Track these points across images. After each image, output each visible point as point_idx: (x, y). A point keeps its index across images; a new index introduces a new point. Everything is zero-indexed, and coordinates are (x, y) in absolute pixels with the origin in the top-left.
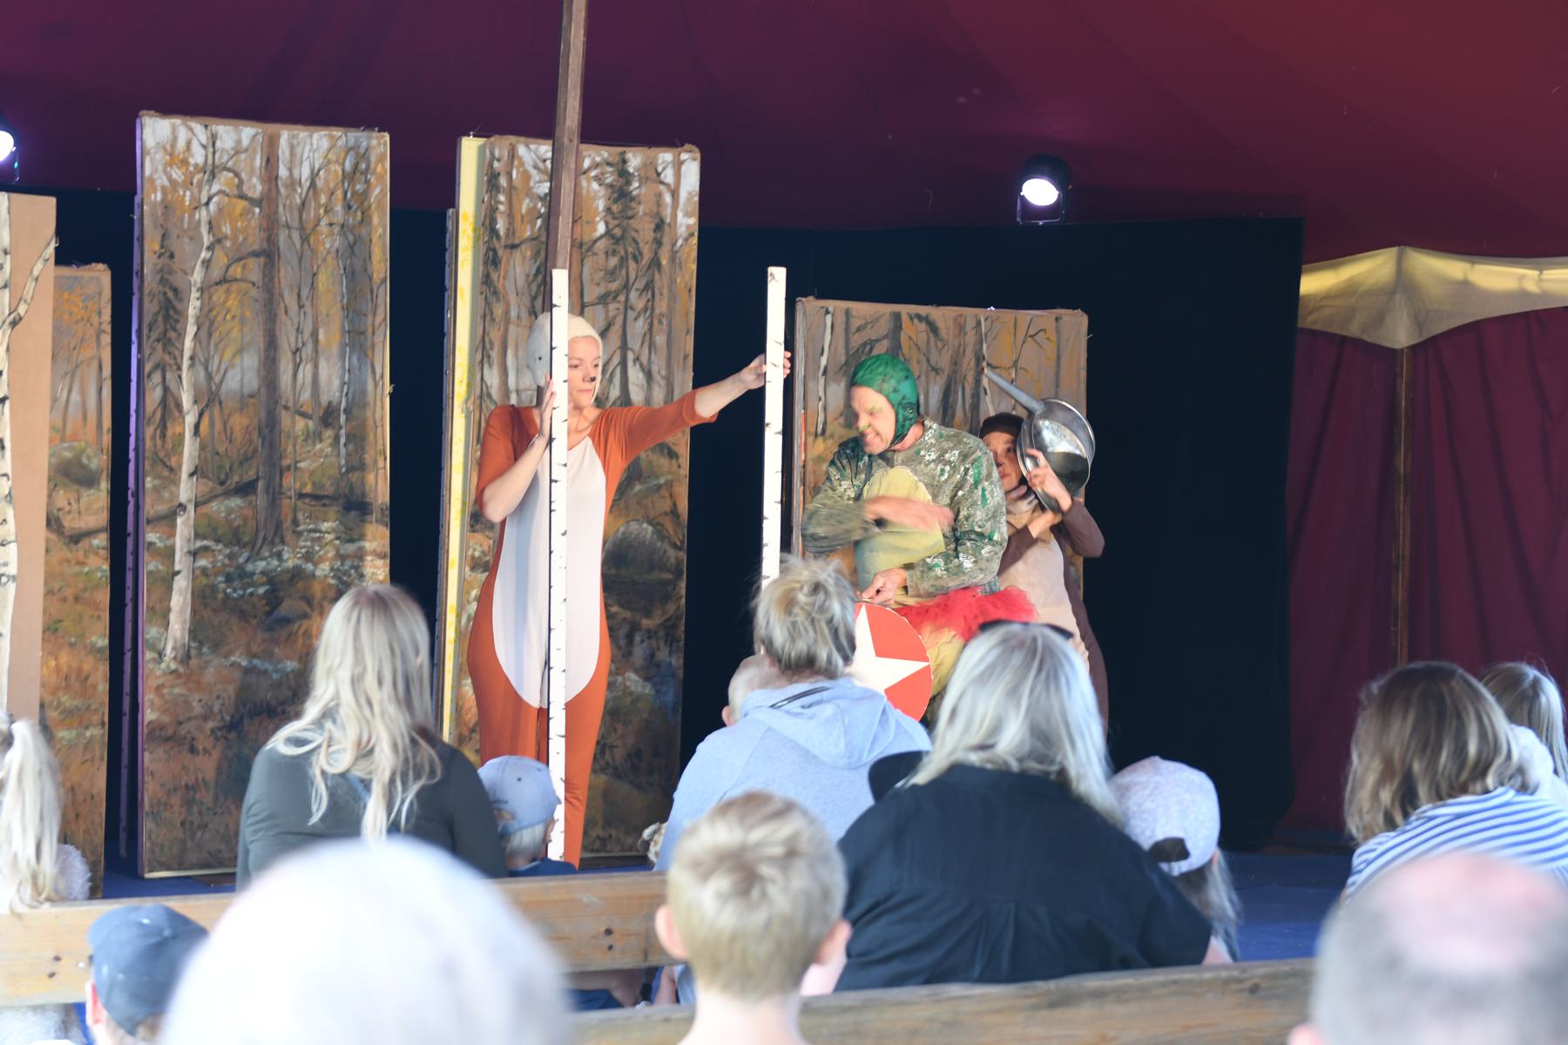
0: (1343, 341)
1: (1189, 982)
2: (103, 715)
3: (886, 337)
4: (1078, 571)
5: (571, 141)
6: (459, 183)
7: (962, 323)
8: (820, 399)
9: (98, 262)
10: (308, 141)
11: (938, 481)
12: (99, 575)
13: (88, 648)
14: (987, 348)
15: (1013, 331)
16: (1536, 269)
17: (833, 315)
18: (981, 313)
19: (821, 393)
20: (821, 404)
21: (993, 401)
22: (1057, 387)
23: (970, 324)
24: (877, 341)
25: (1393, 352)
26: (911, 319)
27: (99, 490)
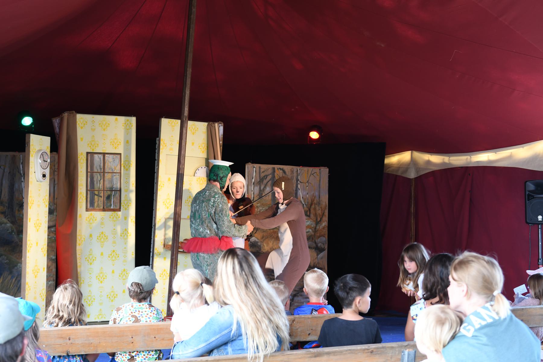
0: (396, 176)
1: (354, 350)
2: (54, 278)
3: (271, 174)
4: (326, 239)
5: (186, 119)
6: (161, 131)
7: (293, 170)
9: (54, 152)
10: (56, 122)
12: (53, 238)
14: (300, 177)
15: (307, 173)
17: (256, 168)
18: (298, 168)
19: (253, 189)
20: (252, 192)
21: (301, 192)
22: (320, 188)
23: (295, 171)
25: (410, 179)
26: (278, 169)
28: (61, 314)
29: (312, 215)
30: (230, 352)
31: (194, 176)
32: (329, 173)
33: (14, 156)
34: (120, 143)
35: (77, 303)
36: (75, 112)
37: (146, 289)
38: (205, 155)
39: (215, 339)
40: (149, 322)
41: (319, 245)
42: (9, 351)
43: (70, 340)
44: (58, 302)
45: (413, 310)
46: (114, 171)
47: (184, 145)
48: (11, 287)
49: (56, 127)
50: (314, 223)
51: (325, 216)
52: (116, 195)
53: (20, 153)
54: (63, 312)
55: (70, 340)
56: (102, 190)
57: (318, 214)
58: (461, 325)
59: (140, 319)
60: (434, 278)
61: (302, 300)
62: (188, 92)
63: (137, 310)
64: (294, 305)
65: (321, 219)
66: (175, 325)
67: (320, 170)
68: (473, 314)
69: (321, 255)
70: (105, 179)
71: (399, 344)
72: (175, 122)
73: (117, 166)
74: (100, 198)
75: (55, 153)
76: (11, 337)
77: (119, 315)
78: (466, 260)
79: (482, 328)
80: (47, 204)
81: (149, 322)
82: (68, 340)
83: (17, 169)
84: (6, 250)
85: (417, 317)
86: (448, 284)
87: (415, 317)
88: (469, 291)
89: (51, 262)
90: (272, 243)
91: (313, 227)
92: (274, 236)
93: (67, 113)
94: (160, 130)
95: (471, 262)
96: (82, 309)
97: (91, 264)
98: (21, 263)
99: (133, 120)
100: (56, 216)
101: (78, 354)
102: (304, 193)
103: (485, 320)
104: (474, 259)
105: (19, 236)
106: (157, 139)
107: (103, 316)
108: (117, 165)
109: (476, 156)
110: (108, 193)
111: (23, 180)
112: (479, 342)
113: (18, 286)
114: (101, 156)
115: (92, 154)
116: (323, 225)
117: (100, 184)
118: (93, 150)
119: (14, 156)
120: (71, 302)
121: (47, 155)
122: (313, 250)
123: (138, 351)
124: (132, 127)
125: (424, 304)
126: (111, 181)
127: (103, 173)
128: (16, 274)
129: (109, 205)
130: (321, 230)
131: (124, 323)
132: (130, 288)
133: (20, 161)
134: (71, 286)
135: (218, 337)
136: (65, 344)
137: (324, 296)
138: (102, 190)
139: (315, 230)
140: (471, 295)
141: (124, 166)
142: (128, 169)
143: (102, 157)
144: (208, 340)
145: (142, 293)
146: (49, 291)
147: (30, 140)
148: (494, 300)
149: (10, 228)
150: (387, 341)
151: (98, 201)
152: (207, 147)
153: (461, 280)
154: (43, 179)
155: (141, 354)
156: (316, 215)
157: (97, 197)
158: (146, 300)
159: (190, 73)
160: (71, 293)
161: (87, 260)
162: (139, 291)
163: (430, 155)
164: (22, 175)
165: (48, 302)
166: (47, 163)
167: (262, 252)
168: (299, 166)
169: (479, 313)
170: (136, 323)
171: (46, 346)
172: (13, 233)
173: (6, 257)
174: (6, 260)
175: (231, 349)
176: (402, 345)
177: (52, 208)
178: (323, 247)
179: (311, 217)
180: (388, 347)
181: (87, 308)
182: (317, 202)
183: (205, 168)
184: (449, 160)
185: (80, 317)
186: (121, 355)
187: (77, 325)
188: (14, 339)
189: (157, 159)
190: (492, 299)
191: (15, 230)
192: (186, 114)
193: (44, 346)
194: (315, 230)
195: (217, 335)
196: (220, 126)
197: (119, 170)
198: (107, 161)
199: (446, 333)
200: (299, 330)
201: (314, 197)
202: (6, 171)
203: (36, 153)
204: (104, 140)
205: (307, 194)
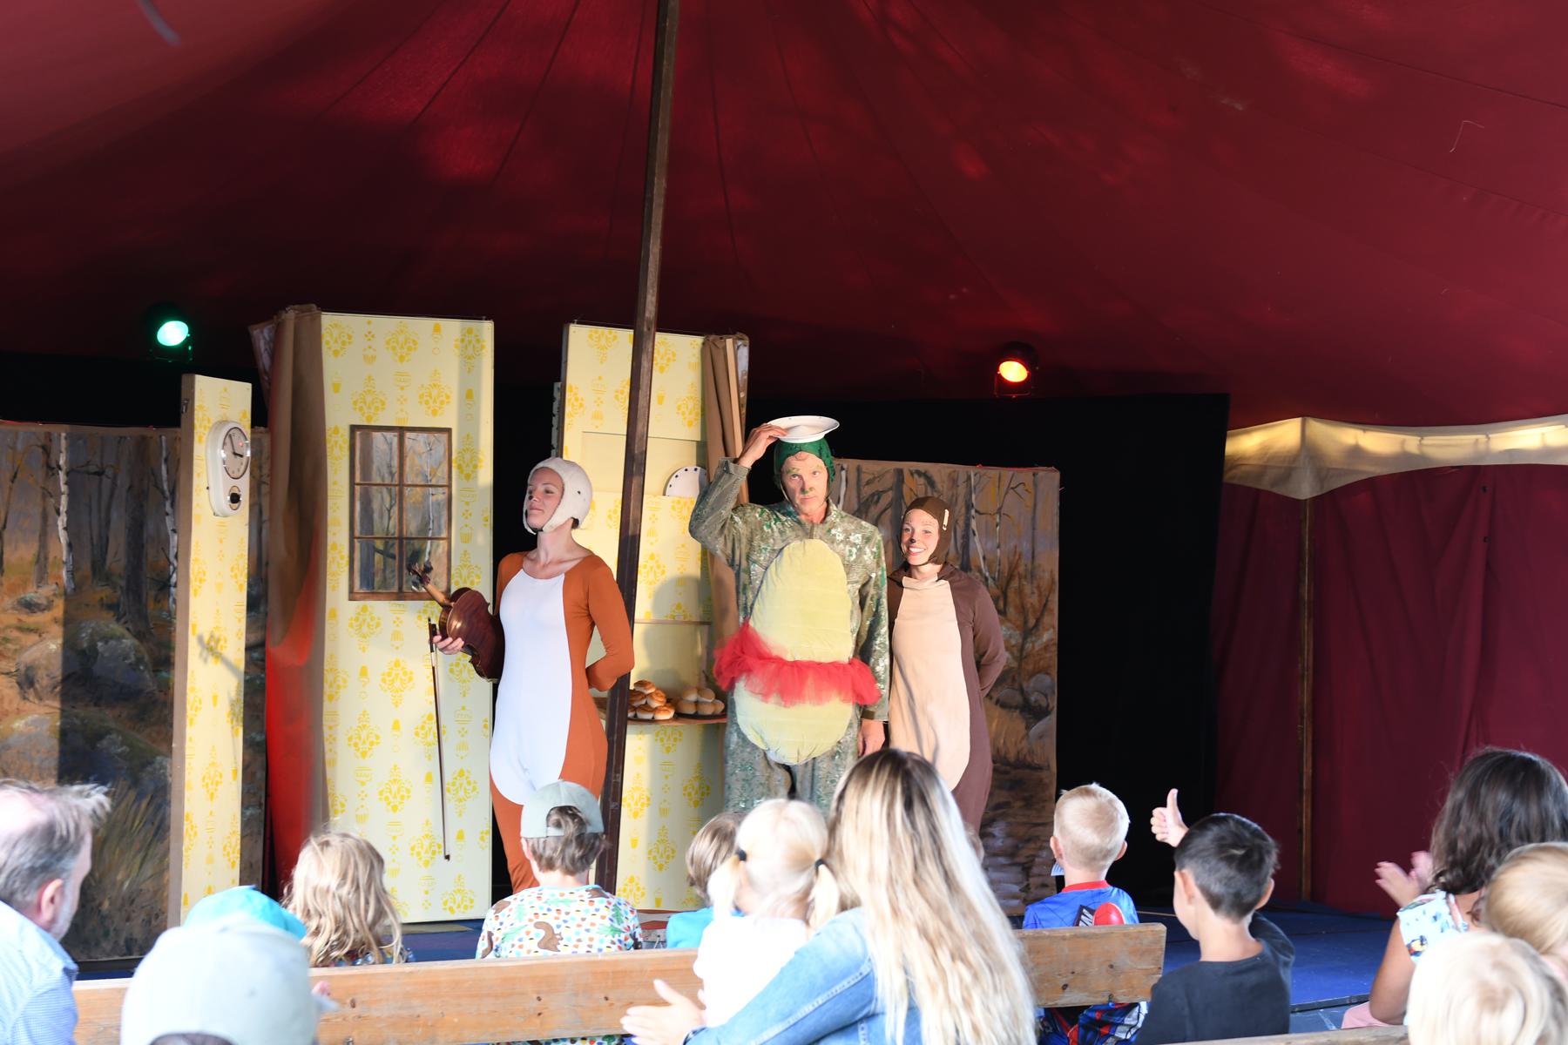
0: (1257, 494)
2: (261, 797)
3: (891, 489)
4: (1053, 679)
5: (649, 329)
6: (566, 362)
9: (260, 426)
10: (261, 337)
11: (849, 561)
12: (258, 682)
14: (976, 498)
17: (847, 471)
18: (972, 470)
22: (1034, 529)
23: (962, 478)
24: (883, 492)
25: (1297, 502)
26: (912, 474)
29: (1011, 611)
31: (664, 495)
32: (1062, 483)
33: (143, 442)
34: (448, 397)
35: (363, 881)
36: (318, 306)
41: (1033, 698)
43: (354, 1006)
46: (431, 480)
47: (645, 405)
48: (136, 825)
49: (263, 350)
50: (1018, 632)
51: (1051, 611)
52: (435, 552)
55: (354, 1006)
59: (560, 934)
60: (1481, 828)
63: (554, 908)
65: (1038, 621)
67: (1034, 475)
69: (1039, 727)
70: (404, 505)
74: (390, 560)
75: (262, 429)
77: (501, 924)
82: (348, 1009)
84: (120, 716)
85: (1424, 947)
87: (1416, 946)
91: (1013, 646)
93: (295, 310)
97: (364, 754)
99: (486, 329)
102: (989, 545)
106: (557, 385)
110: (413, 544)
111: (168, 508)
113: (156, 823)
114: (393, 437)
115: (366, 431)
116: (1044, 640)
117: (390, 518)
118: (369, 418)
119: (144, 438)
120: (344, 877)
122: (1016, 713)
124: (481, 350)
127: (397, 488)
128: (151, 787)
133: (161, 454)
135: (820, 1002)
136: (339, 1020)
138: (395, 538)
139: (1021, 655)
141: (459, 467)
143: (395, 441)
144: (790, 1015)
147: (193, 394)
149: (134, 652)
151: (384, 570)
154: (231, 508)
156: (1022, 609)
157: (382, 557)
159: (663, 192)
160: (342, 853)
163: (1361, 429)
164: (167, 494)
166: (244, 460)
168: (974, 464)
174: (122, 745)
176: (1387, 1036)
178: (1044, 704)
179: (1008, 615)
182: (1026, 570)
184: (1421, 445)
189: (555, 446)
191: (147, 658)
192: (650, 313)
194: (1021, 655)
195: (818, 995)
196: (738, 347)
197: (446, 477)
198: (411, 452)
201: (1017, 557)
202: (119, 482)
203: (210, 432)
204: (402, 388)
205: (999, 547)
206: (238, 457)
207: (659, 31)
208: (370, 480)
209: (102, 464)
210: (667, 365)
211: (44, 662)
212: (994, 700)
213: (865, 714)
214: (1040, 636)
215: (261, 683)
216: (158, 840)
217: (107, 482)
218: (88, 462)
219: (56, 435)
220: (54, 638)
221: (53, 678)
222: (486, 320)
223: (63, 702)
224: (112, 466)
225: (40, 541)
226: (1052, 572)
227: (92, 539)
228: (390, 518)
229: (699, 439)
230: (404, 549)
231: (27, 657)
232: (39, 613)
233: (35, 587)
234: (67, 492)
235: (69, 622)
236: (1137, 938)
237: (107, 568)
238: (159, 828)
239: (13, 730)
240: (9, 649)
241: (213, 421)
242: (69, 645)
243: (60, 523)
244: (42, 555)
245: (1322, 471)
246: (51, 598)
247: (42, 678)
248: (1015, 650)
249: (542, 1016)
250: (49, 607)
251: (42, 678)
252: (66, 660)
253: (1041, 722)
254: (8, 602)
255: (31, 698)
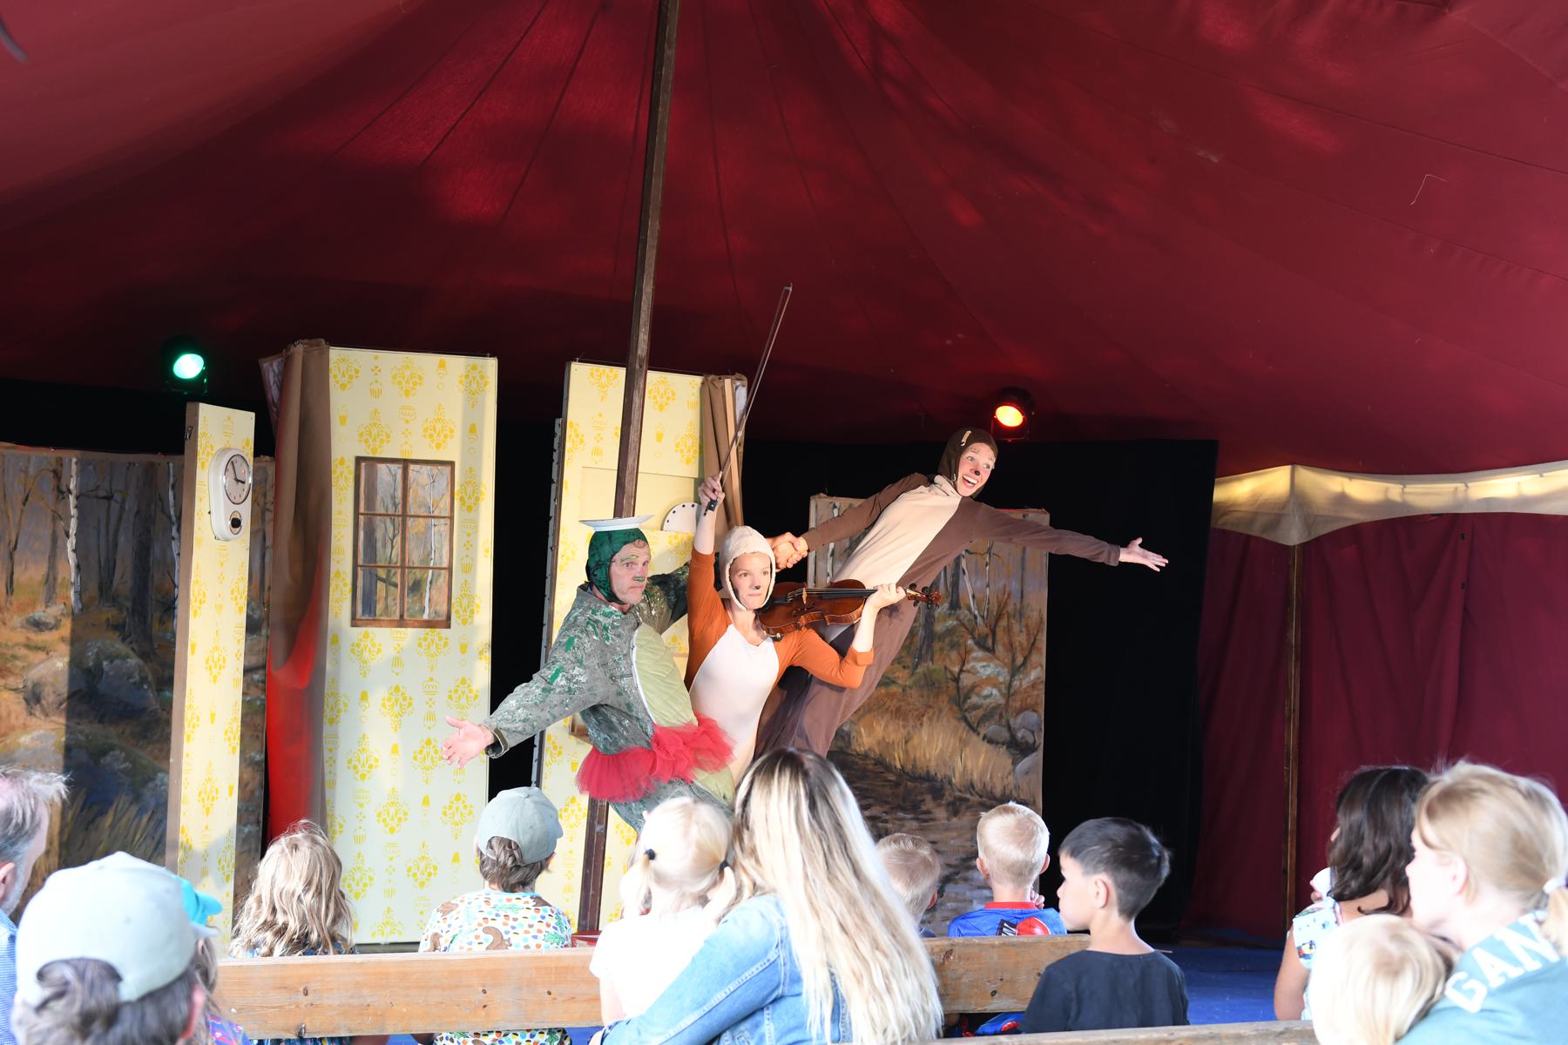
0: (1248, 537)
4: (1039, 716)
5: (641, 367)
6: (568, 398)
8: (828, 575)
10: (271, 370)
12: (258, 703)
13: (248, 761)
16: (1401, 484)
19: (829, 571)
22: (1023, 569)
25: (1287, 547)
27: (260, 635)
28: (280, 919)
29: (1000, 649)
30: (770, 1033)
31: (662, 529)
35: (325, 888)
37: (528, 859)
38: (694, 472)
39: (724, 996)
40: (533, 947)
41: (1019, 735)
42: (153, 1023)
44: (273, 884)
45: (1300, 929)
47: (637, 439)
48: (137, 839)
49: (272, 383)
50: (1006, 670)
51: (1039, 650)
52: (437, 580)
53: (169, 458)
54: (285, 912)
55: (306, 994)
56: (397, 567)
57: (1017, 644)
58: (1447, 979)
61: (968, 894)
62: (648, 289)
64: (943, 908)
65: (1026, 659)
66: (603, 957)
68: (1481, 945)
69: (1026, 763)
70: (407, 534)
71: (1260, 1028)
72: (610, 374)
73: (441, 499)
74: (392, 588)
75: (267, 458)
76: (160, 981)
77: (449, 926)
78: (1461, 787)
79: (1511, 986)
80: (243, 602)
81: (533, 947)
83: (160, 503)
84: (123, 733)
85: (1312, 951)
86: (1408, 854)
87: (1306, 950)
88: (1472, 880)
89: (250, 769)
90: (883, 725)
91: (1001, 683)
92: (890, 707)
94: (565, 397)
95: (1478, 794)
96: (340, 906)
97: (363, 777)
98: (167, 772)
99: (490, 365)
100: (268, 637)
101: (329, 1036)
102: (979, 584)
103: (1516, 962)
104: (1486, 786)
105: (163, 693)
106: (559, 421)
107: (395, 929)
108: (443, 495)
109: (1476, 483)
112: (1502, 1028)
113: (157, 837)
114: (397, 469)
115: (370, 463)
117: (392, 547)
118: (374, 450)
119: (152, 465)
120: (309, 884)
121: (244, 465)
123: (500, 1032)
124: (485, 385)
125: (1335, 912)
126: (425, 539)
127: (400, 519)
128: (152, 803)
129: (417, 608)
130: (1026, 692)
131: (461, 948)
132: (483, 852)
134: (309, 840)
135: (732, 989)
136: (293, 1007)
137: (1035, 884)
138: (397, 567)
140: (1477, 891)
141: (462, 499)
142: (472, 507)
143: (399, 473)
145: (518, 867)
146: (245, 852)
148: (1546, 905)
149: (138, 672)
150: (1217, 1017)
151: (386, 598)
152: (701, 447)
153: (1449, 847)
155: (509, 1039)
156: (1010, 647)
158: (527, 888)
160: (310, 861)
161: (352, 765)
162: (509, 863)
163: (1347, 477)
164: (174, 519)
165: (243, 885)
166: (246, 486)
167: (854, 753)
169: (1501, 944)
170: (496, 951)
171: (240, 1010)
172: (145, 687)
173: (123, 754)
174: (125, 762)
175: (772, 1024)
176: (1267, 1030)
177: (256, 616)
178: (1031, 740)
180: (1227, 1037)
181: (355, 904)
182: (1015, 609)
183: (693, 506)
184: (1403, 493)
185: (335, 928)
186: (452, 1040)
187: (326, 953)
188: (167, 988)
190: (1539, 902)
191: (150, 678)
193: (233, 1010)
194: (1009, 690)
198: (415, 483)
199: (1404, 1000)
200: (964, 980)
201: (1006, 596)
202: (127, 507)
204: (407, 422)
205: (988, 586)
206: (240, 484)
207: (655, 79)
208: (374, 509)
209: (111, 489)
210: (666, 404)
211: (50, 679)
212: (982, 736)
213: (977, 793)
214: (1028, 674)
215: (261, 704)
216: (158, 855)
217: (115, 506)
218: (98, 487)
219: (67, 460)
220: (62, 656)
221: (59, 695)
222: (490, 357)
223: (68, 718)
224: (121, 492)
225: (49, 562)
226: (1040, 611)
227: (100, 561)
228: (392, 547)
229: (697, 476)
230: (406, 578)
231: (34, 674)
232: (46, 632)
233: (43, 608)
234: (76, 515)
235: (75, 641)
236: (1064, 948)
237: (114, 588)
238: (159, 843)
239: (19, 744)
240: (17, 666)
241: (217, 447)
242: (75, 663)
243: (69, 545)
244: (51, 577)
245: (1309, 519)
246: (59, 618)
247: (49, 695)
248: (1003, 688)
249: (486, 1008)
250: (56, 626)
251: (49, 695)
252: (72, 678)
253: (1027, 759)
254: (17, 620)
255: (38, 714)
